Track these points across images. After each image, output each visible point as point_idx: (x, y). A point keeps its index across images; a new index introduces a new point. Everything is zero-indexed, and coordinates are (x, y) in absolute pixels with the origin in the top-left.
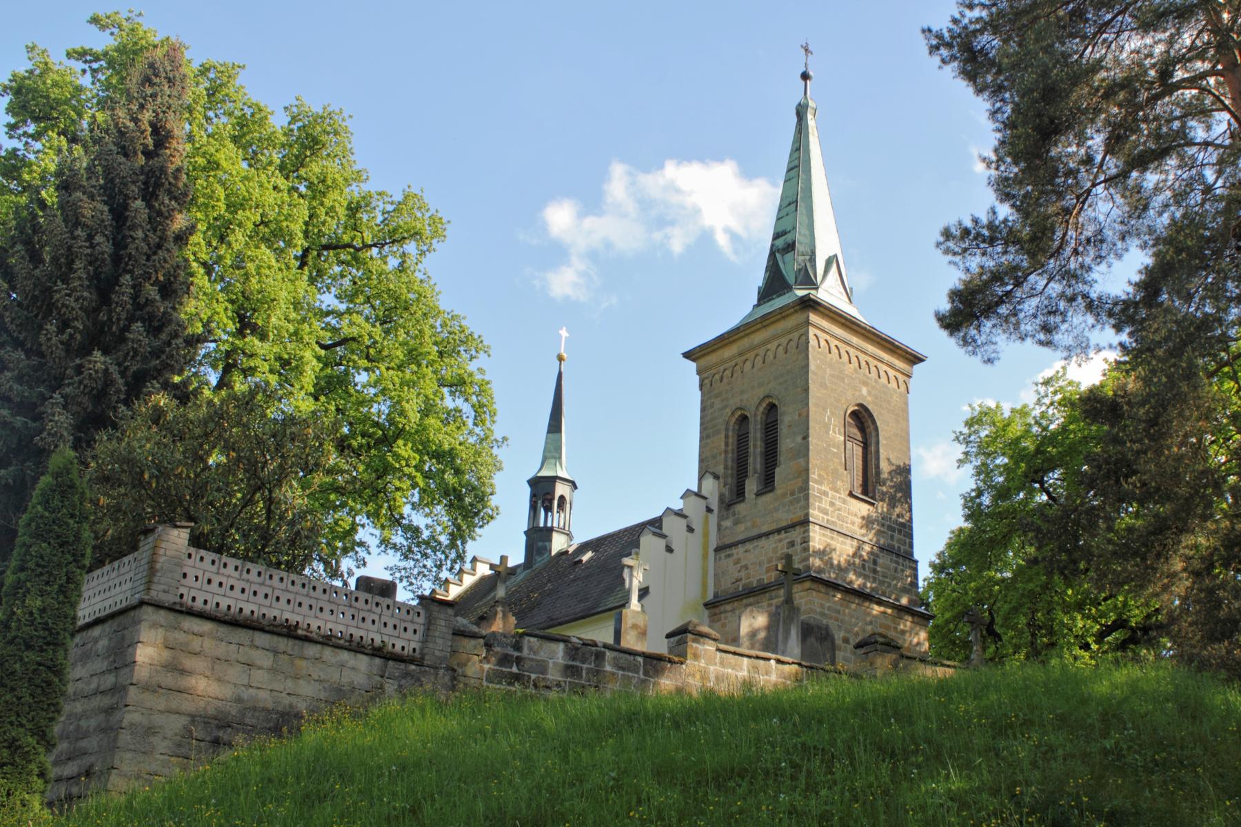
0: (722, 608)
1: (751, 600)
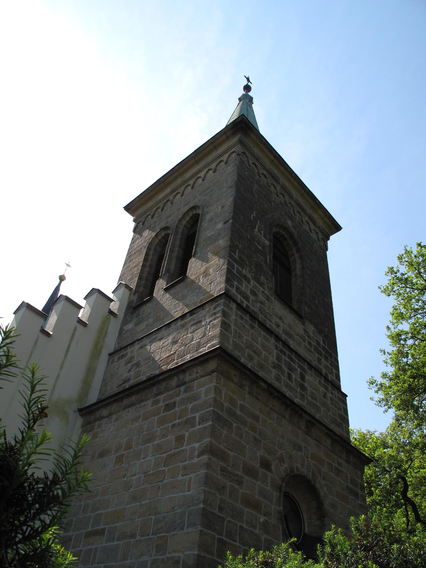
0: (98, 414)
1: (133, 398)
